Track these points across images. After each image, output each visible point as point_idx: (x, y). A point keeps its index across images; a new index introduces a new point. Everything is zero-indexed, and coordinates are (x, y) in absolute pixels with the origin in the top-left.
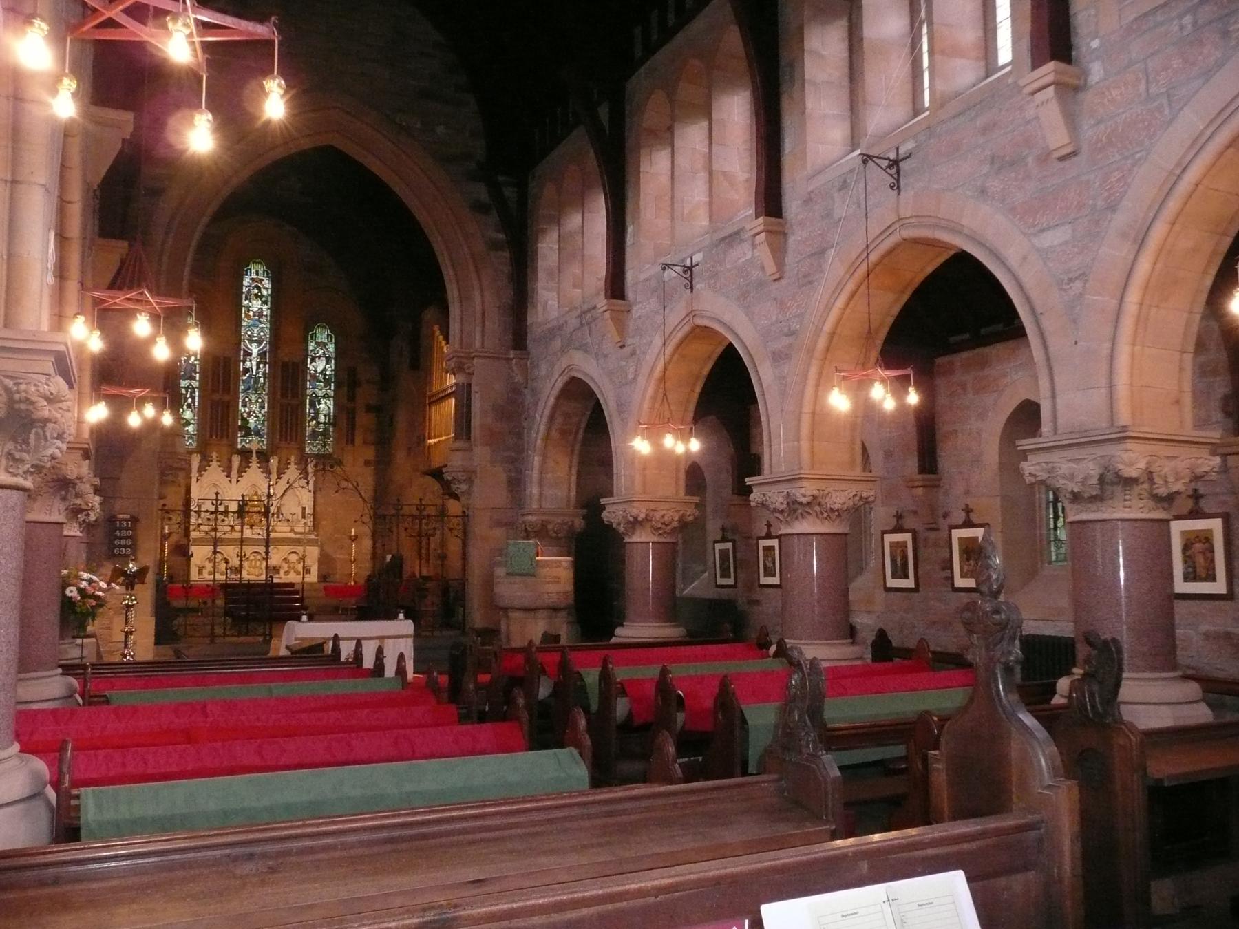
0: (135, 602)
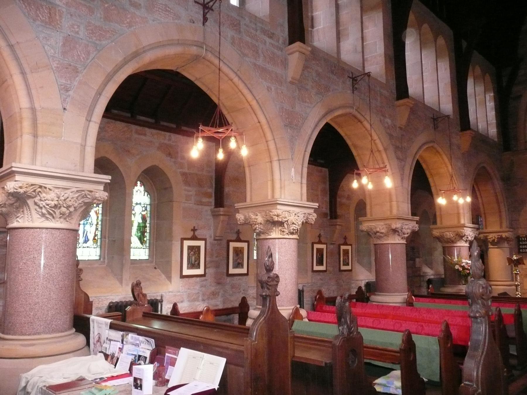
0: (518, 272)
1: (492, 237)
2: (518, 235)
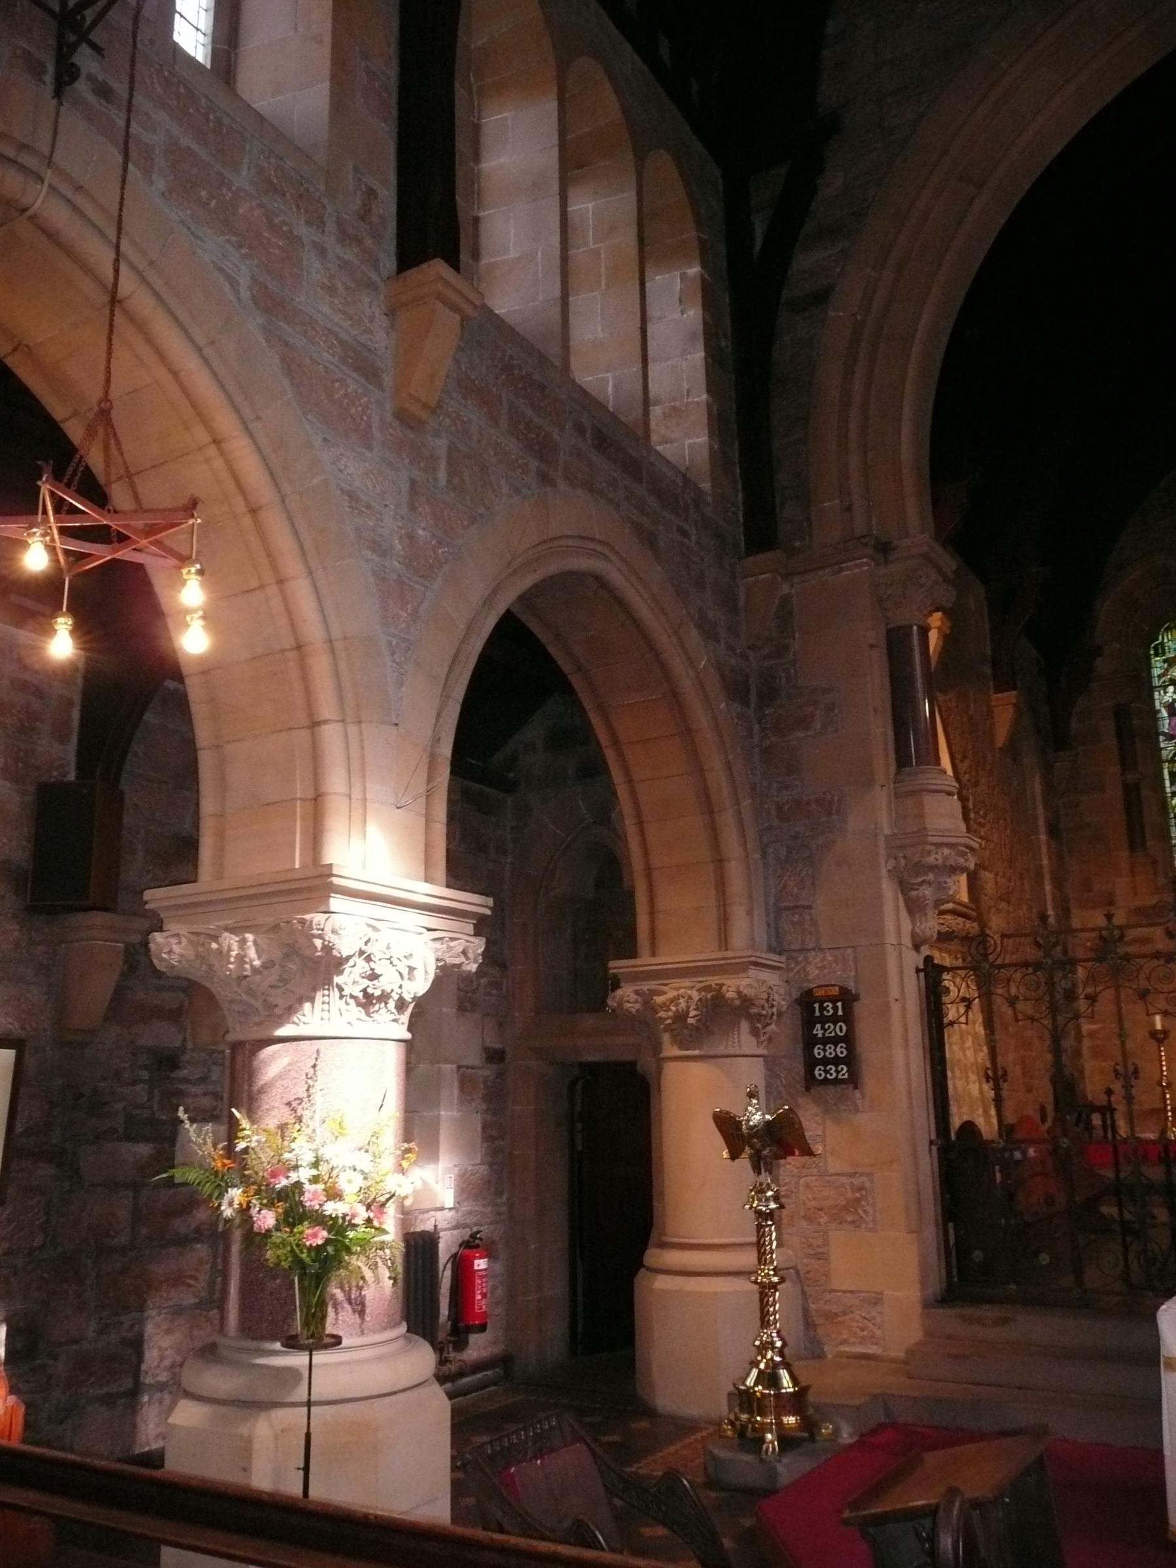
1: (672, 1001)
2: (807, 986)
